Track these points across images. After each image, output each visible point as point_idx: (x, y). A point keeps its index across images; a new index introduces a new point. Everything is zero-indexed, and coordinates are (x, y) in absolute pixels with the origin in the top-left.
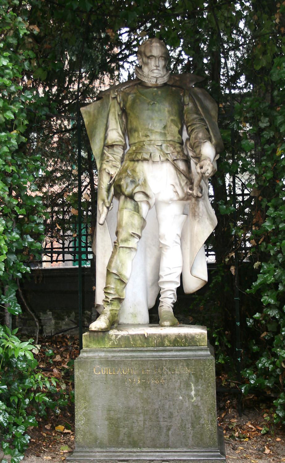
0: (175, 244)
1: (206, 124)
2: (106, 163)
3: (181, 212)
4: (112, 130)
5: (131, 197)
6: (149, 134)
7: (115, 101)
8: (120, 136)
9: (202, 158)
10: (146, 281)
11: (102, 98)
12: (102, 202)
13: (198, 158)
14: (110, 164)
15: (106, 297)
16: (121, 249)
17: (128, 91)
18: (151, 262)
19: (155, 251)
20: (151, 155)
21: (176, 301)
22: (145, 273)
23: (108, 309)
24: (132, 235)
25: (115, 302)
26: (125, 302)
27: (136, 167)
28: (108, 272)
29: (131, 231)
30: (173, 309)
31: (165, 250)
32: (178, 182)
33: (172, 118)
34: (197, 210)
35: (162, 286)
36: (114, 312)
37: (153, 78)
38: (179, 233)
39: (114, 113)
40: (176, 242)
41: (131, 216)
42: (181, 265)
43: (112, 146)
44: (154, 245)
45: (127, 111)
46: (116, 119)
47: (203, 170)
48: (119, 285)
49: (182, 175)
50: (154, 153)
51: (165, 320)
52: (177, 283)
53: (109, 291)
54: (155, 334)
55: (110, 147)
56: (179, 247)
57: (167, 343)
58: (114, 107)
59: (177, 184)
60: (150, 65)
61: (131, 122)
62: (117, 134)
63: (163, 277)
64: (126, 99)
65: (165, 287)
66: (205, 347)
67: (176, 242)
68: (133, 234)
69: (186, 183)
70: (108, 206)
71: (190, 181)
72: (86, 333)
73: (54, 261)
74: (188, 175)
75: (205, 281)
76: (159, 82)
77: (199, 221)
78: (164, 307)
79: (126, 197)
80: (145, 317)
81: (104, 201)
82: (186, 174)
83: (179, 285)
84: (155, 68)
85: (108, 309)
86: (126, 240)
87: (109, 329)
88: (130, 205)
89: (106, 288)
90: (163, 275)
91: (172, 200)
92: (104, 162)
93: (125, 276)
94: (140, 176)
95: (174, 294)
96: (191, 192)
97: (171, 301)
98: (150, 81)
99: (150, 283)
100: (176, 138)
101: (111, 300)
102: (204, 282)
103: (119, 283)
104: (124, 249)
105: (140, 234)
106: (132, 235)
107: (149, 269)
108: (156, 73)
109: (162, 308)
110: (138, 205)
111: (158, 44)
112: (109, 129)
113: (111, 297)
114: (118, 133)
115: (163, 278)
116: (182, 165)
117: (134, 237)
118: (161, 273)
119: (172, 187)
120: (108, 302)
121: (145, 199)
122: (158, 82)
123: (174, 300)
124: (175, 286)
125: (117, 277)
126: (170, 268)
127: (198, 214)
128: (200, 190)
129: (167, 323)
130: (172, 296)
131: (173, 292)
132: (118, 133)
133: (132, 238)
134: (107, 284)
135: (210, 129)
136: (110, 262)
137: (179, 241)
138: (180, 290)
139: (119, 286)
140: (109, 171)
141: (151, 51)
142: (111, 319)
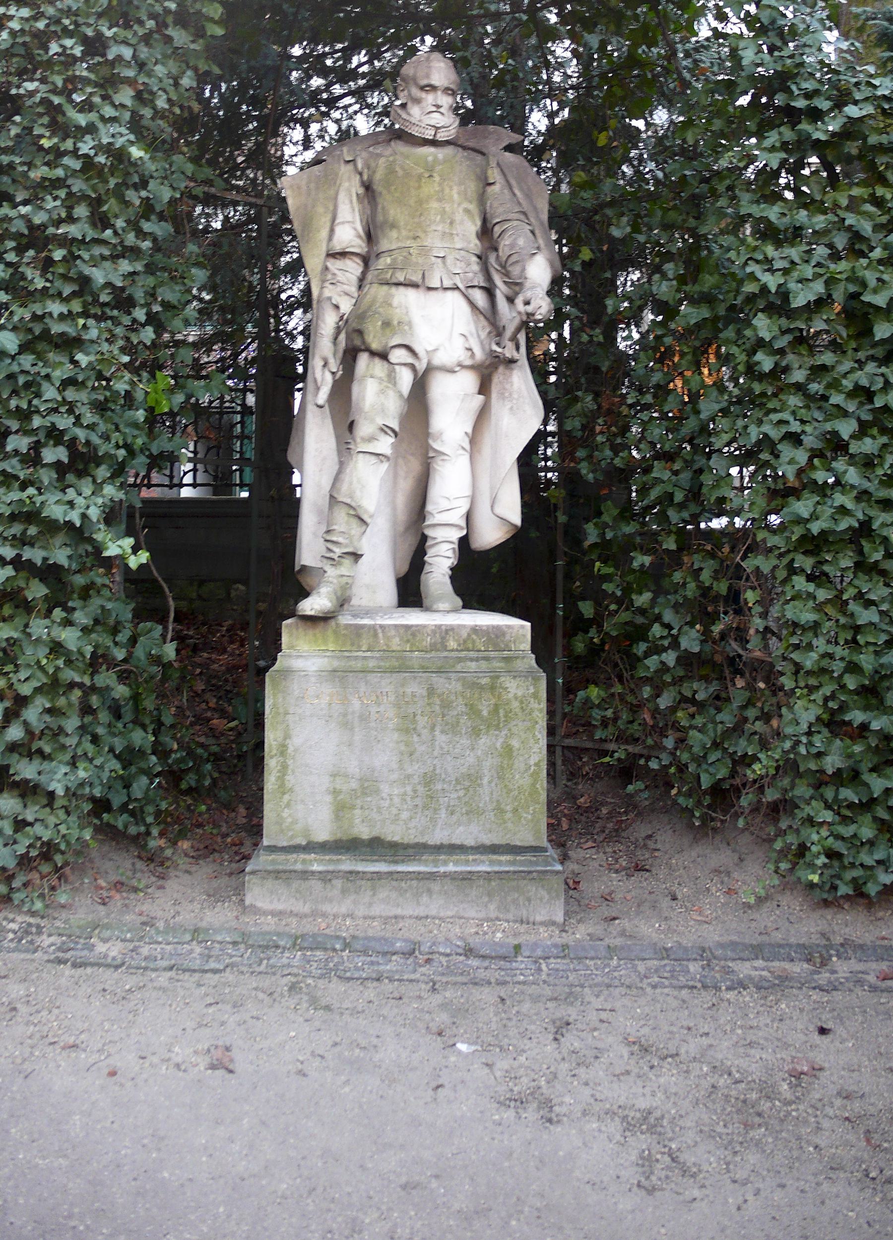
0: (462, 452)
2: (331, 287)
3: (476, 390)
4: (343, 223)
5: (383, 356)
6: (420, 234)
7: (350, 167)
8: (360, 237)
9: (528, 285)
10: (394, 523)
12: (322, 363)
13: (516, 286)
14: (339, 289)
15: (329, 550)
16: (361, 455)
18: (406, 485)
19: (415, 466)
22: (394, 509)
23: (331, 572)
24: (382, 430)
25: (347, 562)
26: (361, 561)
27: (393, 296)
28: (333, 500)
29: (380, 422)
30: (451, 577)
31: (440, 463)
32: (474, 331)
33: (466, 205)
34: (508, 386)
35: (429, 532)
36: (345, 580)
38: (470, 431)
39: (349, 191)
40: (463, 448)
41: (382, 392)
42: (468, 492)
43: (343, 254)
44: (412, 454)
45: (375, 187)
46: (351, 202)
47: (529, 309)
48: (354, 526)
49: (482, 318)
50: (94, 369)
51: (440, 598)
52: (461, 528)
53: (334, 539)
54: (424, 626)
56: (466, 457)
57: (452, 644)
58: (349, 179)
59: (472, 334)
60: (424, 104)
61: (383, 208)
62: (353, 232)
64: (373, 165)
67: (463, 448)
69: (490, 333)
70: (334, 370)
71: (497, 331)
72: (289, 621)
73: (176, 485)
74: (491, 316)
75: (516, 526)
77: (511, 408)
78: (434, 575)
79: (373, 354)
80: (388, 592)
82: (489, 315)
83: (464, 532)
84: (434, 109)
85: (331, 572)
86: (371, 439)
88: (379, 366)
89: (328, 532)
90: (434, 512)
91: (463, 367)
92: (327, 284)
93: (366, 511)
94: (397, 315)
96: (499, 350)
99: (401, 529)
100: (472, 245)
102: (511, 528)
103: (354, 522)
104: (368, 456)
107: (402, 500)
109: (431, 576)
110: (394, 371)
111: (442, 65)
112: (337, 221)
113: (338, 551)
114: (355, 229)
116: (479, 297)
117: (386, 433)
118: (429, 507)
119: (462, 339)
120: (333, 559)
121: (410, 360)
122: (438, 135)
124: (456, 535)
125: (352, 512)
127: (511, 394)
129: (442, 606)
130: (450, 554)
131: (452, 546)
133: (383, 434)
134: (329, 524)
136: (337, 479)
137: (468, 447)
138: (464, 543)
139: (355, 528)
141: (428, 76)
142: (339, 593)
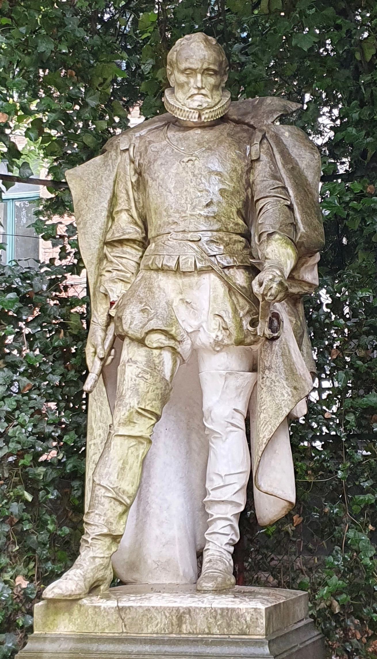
1: (290, 196)
11: (106, 150)
17: (150, 138)
20: (179, 258)
21: (237, 540)
24: (139, 413)
37: (193, 111)
55: (116, 244)
63: (211, 492)
65: (215, 511)
66: (260, 637)
68: (140, 411)
75: (290, 503)
76: (205, 118)
81: (95, 347)
87: (81, 596)
95: (231, 526)
97: (226, 540)
98: (188, 117)
101: (93, 539)
105: (158, 412)
106: (139, 413)
108: (197, 101)
114: (132, 216)
115: (210, 494)
123: (234, 537)
126: (220, 476)
128: (133, 337)
130: (228, 530)
131: (229, 523)
132: (132, 216)
135: (295, 207)
140: (106, 291)
